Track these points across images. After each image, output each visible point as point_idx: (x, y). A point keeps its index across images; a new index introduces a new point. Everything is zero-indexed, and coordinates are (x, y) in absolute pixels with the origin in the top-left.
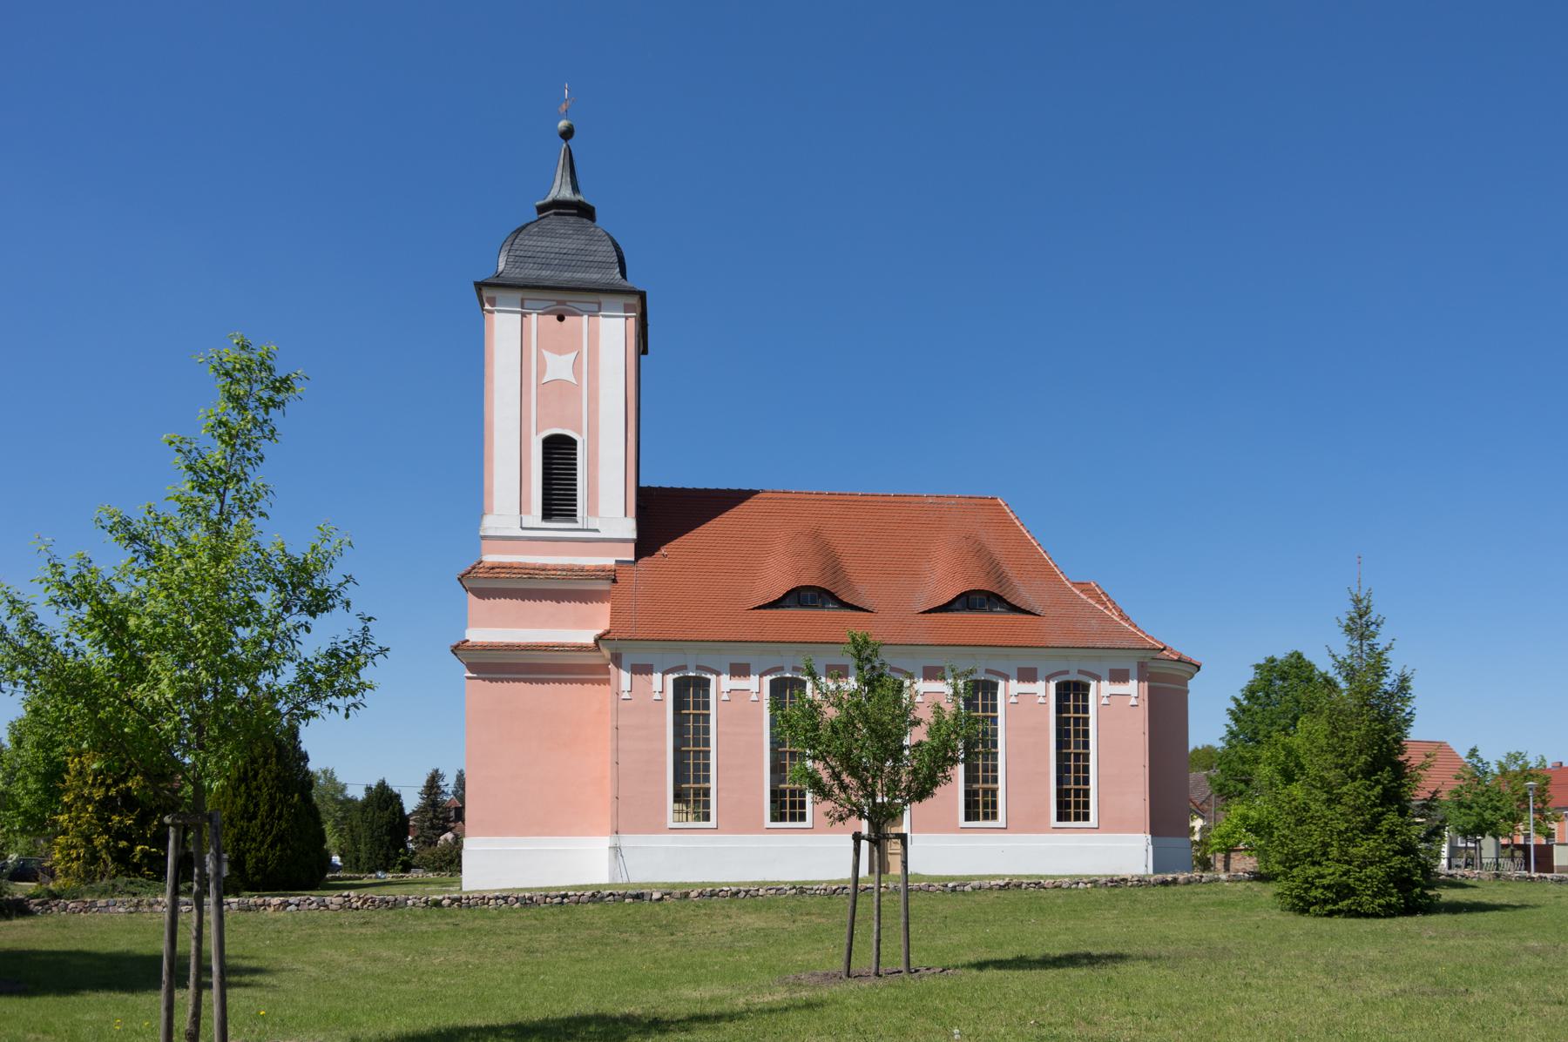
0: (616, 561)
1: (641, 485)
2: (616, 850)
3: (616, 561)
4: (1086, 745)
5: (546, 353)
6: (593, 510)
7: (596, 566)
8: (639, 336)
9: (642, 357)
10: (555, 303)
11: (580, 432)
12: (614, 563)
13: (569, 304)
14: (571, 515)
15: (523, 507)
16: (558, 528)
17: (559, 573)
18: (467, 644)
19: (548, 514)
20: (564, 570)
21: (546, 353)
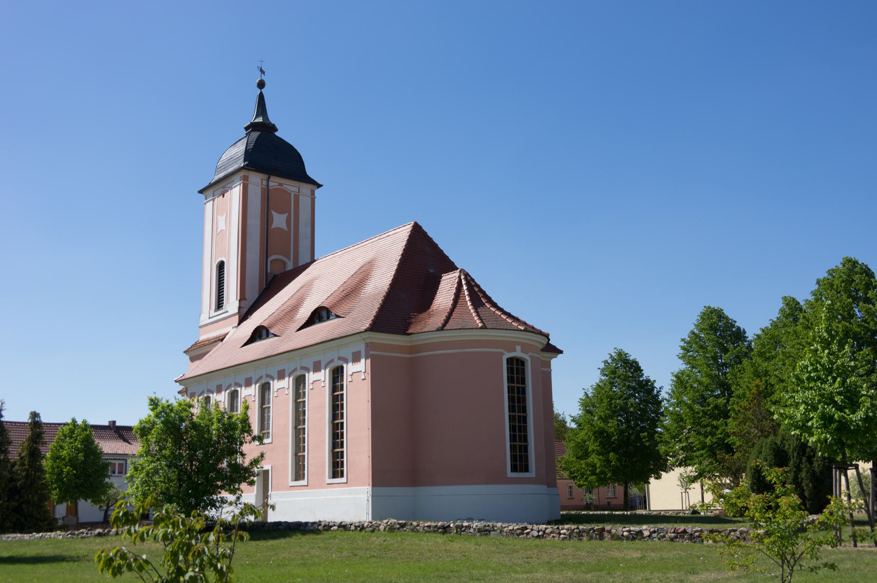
13: (284, 185)
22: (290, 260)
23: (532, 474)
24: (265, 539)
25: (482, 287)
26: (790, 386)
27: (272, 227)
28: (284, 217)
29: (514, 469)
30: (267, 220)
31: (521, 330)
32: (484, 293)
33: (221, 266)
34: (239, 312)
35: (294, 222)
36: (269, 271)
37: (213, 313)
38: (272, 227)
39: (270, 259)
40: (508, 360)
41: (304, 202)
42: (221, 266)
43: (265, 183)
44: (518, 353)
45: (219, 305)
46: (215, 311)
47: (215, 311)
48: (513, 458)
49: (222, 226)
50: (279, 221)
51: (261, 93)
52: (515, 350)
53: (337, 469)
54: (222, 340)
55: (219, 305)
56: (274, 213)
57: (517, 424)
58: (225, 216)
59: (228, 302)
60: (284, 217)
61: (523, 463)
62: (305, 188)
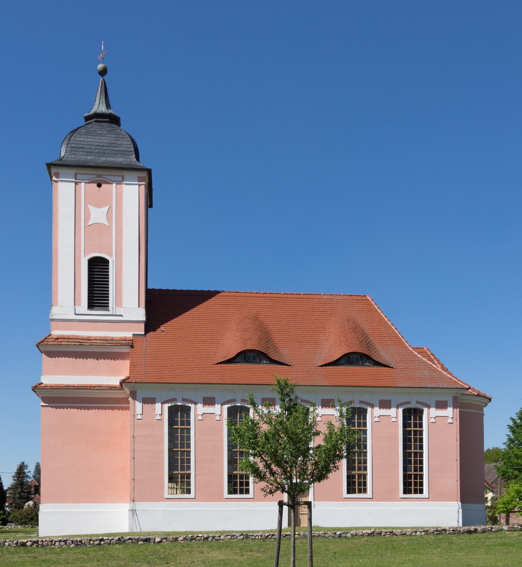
0: (133, 334)
1: (149, 288)
2: (133, 512)
3: (133, 334)
4: (421, 447)
5: (90, 207)
6: (119, 303)
7: (121, 337)
8: (147, 196)
9: (149, 209)
10: (95, 176)
11: (111, 256)
12: (131, 335)
13: (104, 176)
14: (105, 306)
16: (97, 314)
17: (98, 342)
18: (42, 385)
19: (91, 306)
20: (101, 340)
21: (90, 207)
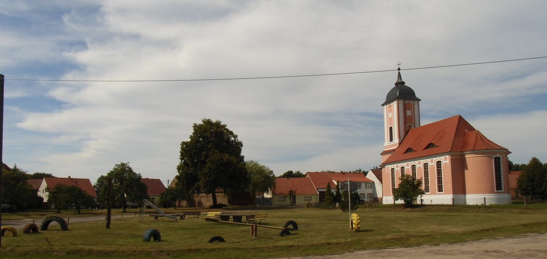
15: (388, 141)
22: (412, 125)
23: (503, 191)
24: (416, 208)
25: (482, 133)
26: (259, 249)
27: (407, 115)
28: (410, 111)
29: (497, 189)
30: (405, 113)
31: (498, 149)
32: (485, 137)
33: (391, 128)
34: (399, 143)
35: (413, 113)
36: (407, 129)
37: (389, 142)
38: (407, 115)
39: (407, 125)
40: (494, 158)
41: (416, 106)
42: (391, 128)
43: (404, 102)
44: (498, 156)
45: (391, 140)
46: (390, 142)
47: (390, 142)
48: (497, 186)
49: (390, 116)
50: (409, 113)
51: (399, 72)
52: (497, 155)
53: (440, 189)
54: (394, 151)
55: (391, 140)
56: (407, 111)
57: (498, 176)
58: (391, 113)
59: (394, 139)
60: (410, 111)
61: (341, 225)
62: (416, 102)
